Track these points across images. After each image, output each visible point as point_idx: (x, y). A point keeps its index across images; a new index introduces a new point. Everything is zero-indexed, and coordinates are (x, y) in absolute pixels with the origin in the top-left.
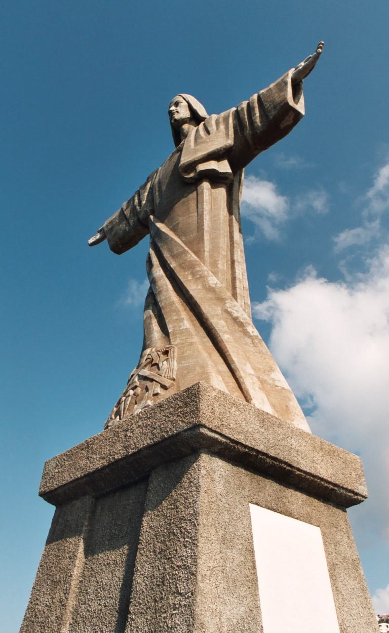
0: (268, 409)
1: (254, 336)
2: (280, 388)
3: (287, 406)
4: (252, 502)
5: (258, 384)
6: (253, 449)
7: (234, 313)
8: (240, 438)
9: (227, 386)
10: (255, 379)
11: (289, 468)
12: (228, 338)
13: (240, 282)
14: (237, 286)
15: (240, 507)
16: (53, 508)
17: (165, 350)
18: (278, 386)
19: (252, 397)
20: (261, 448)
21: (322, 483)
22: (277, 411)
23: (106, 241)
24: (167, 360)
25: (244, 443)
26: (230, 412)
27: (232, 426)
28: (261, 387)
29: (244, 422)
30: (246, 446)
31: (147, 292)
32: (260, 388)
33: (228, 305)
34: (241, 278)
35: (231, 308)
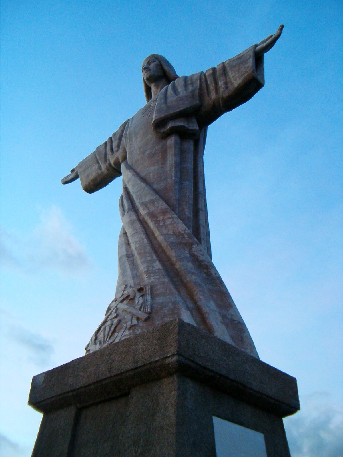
0: (227, 339)
1: (216, 277)
2: (236, 322)
3: (242, 337)
4: (214, 415)
5: (220, 319)
6: (217, 373)
7: (200, 257)
8: (209, 365)
9: (195, 320)
10: (218, 315)
11: (139, 370)
12: (196, 279)
13: (204, 228)
14: (201, 232)
15: (206, 419)
16: (39, 416)
17: (140, 287)
18: (235, 321)
19: (215, 331)
20: (224, 372)
21: (128, 374)
22: (234, 341)
23: (78, 180)
24: (142, 296)
25: (211, 368)
26: (200, 343)
27: (202, 354)
28: (222, 321)
29: (211, 351)
30: (212, 371)
31: (119, 233)
32: (221, 322)
33: (193, 250)
34: (204, 224)
35: (197, 252)
